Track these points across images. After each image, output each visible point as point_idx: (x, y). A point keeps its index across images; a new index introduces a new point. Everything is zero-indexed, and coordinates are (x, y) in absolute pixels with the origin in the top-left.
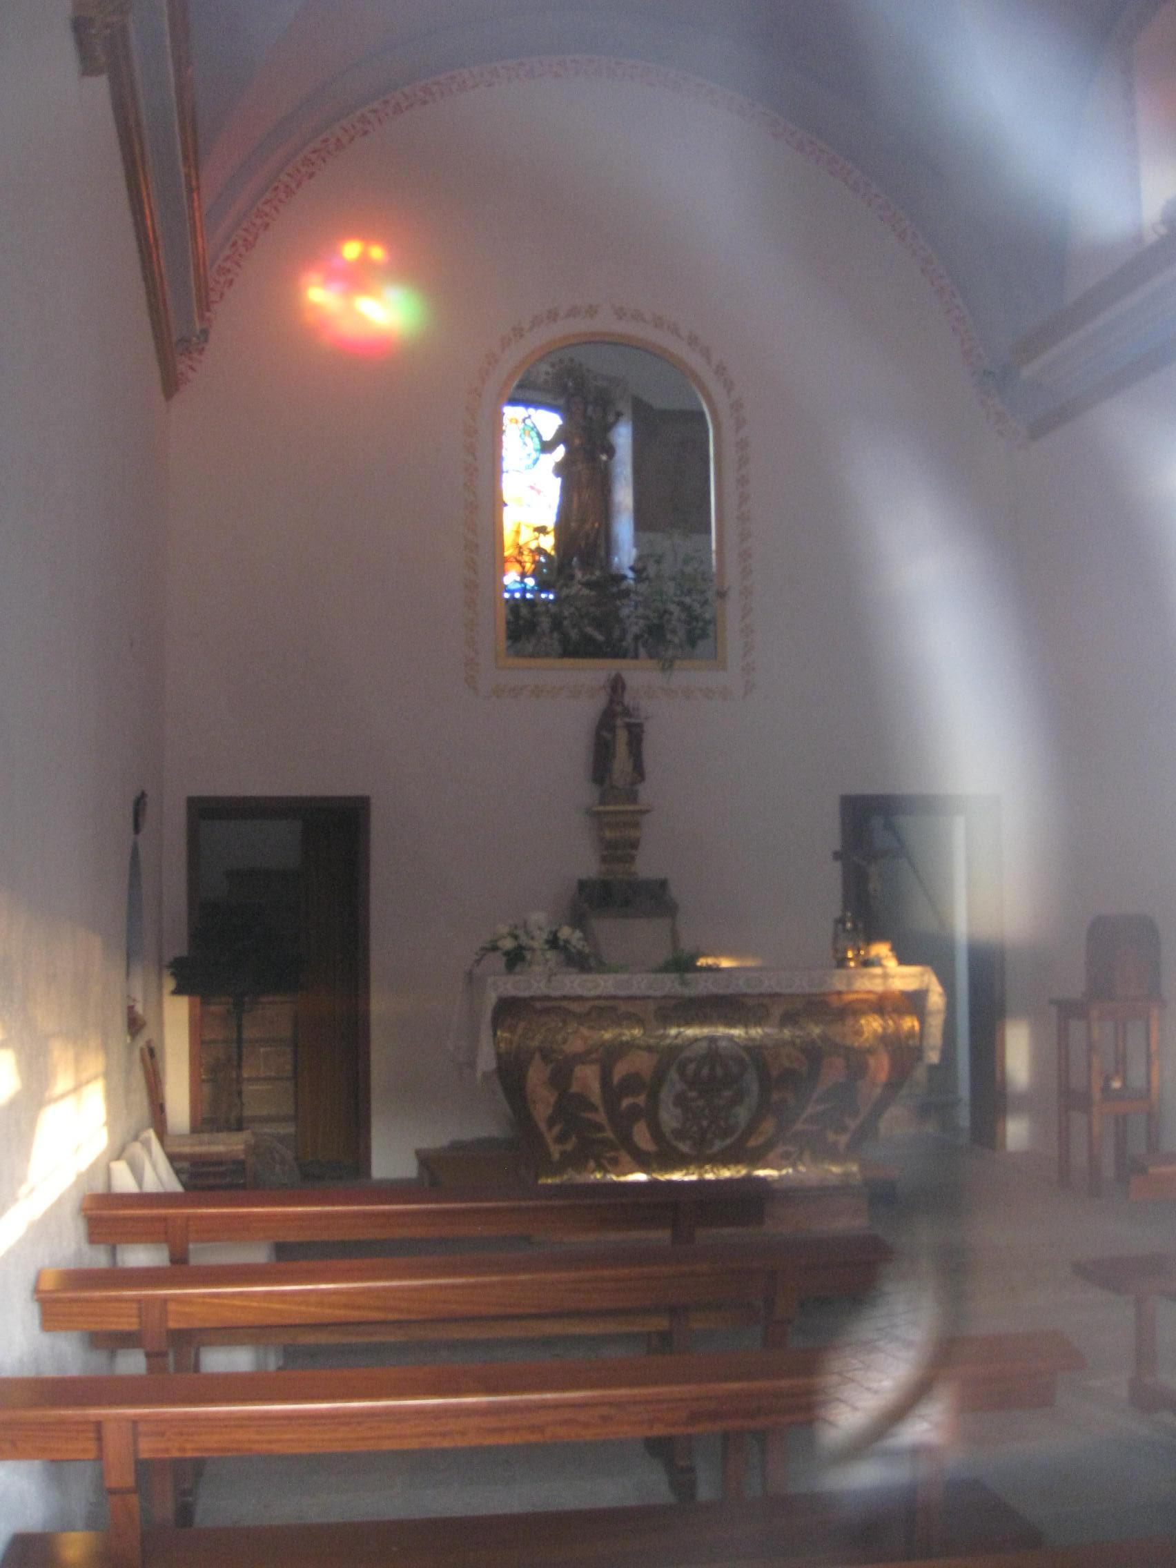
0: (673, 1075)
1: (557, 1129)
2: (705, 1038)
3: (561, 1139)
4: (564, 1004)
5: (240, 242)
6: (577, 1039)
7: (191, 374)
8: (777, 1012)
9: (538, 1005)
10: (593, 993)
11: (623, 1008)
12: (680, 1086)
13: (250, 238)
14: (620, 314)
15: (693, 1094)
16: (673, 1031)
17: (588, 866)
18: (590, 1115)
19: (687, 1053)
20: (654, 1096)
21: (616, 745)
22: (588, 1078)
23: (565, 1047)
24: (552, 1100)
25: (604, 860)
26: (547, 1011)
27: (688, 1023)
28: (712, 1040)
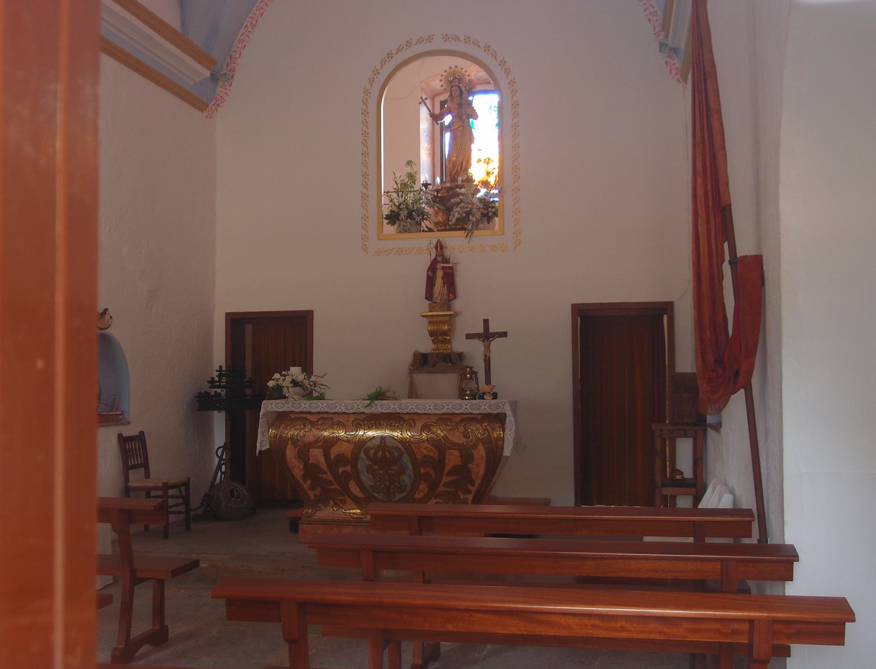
0: (362, 455)
1: (309, 482)
2: (378, 437)
3: (313, 488)
4: (305, 415)
5: (249, 25)
6: (309, 434)
7: (225, 97)
8: (419, 424)
9: (293, 416)
10: (333, 411)
11: (337, 418)
12: (367, 462)
13: (254, 22)
14: (446, 38)
15: (376, 467)
16: (361, 433)
17: (426, 346)
18: (324, 476)
19: (368, 444)
20: (355, 467)
21: (442, 279)
22: (317, 454)
23: (304, 439)
24: (302, 467)
25: (434, 342)
26: (296, 419)
27: (370, 429)
28: (382, 438)
